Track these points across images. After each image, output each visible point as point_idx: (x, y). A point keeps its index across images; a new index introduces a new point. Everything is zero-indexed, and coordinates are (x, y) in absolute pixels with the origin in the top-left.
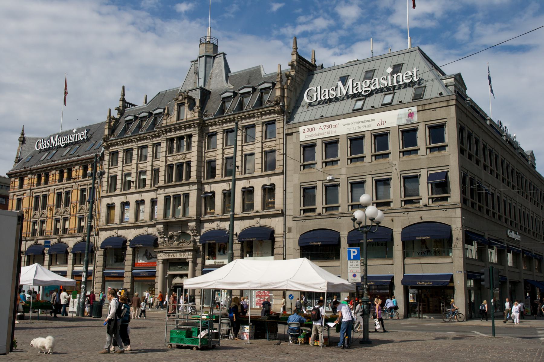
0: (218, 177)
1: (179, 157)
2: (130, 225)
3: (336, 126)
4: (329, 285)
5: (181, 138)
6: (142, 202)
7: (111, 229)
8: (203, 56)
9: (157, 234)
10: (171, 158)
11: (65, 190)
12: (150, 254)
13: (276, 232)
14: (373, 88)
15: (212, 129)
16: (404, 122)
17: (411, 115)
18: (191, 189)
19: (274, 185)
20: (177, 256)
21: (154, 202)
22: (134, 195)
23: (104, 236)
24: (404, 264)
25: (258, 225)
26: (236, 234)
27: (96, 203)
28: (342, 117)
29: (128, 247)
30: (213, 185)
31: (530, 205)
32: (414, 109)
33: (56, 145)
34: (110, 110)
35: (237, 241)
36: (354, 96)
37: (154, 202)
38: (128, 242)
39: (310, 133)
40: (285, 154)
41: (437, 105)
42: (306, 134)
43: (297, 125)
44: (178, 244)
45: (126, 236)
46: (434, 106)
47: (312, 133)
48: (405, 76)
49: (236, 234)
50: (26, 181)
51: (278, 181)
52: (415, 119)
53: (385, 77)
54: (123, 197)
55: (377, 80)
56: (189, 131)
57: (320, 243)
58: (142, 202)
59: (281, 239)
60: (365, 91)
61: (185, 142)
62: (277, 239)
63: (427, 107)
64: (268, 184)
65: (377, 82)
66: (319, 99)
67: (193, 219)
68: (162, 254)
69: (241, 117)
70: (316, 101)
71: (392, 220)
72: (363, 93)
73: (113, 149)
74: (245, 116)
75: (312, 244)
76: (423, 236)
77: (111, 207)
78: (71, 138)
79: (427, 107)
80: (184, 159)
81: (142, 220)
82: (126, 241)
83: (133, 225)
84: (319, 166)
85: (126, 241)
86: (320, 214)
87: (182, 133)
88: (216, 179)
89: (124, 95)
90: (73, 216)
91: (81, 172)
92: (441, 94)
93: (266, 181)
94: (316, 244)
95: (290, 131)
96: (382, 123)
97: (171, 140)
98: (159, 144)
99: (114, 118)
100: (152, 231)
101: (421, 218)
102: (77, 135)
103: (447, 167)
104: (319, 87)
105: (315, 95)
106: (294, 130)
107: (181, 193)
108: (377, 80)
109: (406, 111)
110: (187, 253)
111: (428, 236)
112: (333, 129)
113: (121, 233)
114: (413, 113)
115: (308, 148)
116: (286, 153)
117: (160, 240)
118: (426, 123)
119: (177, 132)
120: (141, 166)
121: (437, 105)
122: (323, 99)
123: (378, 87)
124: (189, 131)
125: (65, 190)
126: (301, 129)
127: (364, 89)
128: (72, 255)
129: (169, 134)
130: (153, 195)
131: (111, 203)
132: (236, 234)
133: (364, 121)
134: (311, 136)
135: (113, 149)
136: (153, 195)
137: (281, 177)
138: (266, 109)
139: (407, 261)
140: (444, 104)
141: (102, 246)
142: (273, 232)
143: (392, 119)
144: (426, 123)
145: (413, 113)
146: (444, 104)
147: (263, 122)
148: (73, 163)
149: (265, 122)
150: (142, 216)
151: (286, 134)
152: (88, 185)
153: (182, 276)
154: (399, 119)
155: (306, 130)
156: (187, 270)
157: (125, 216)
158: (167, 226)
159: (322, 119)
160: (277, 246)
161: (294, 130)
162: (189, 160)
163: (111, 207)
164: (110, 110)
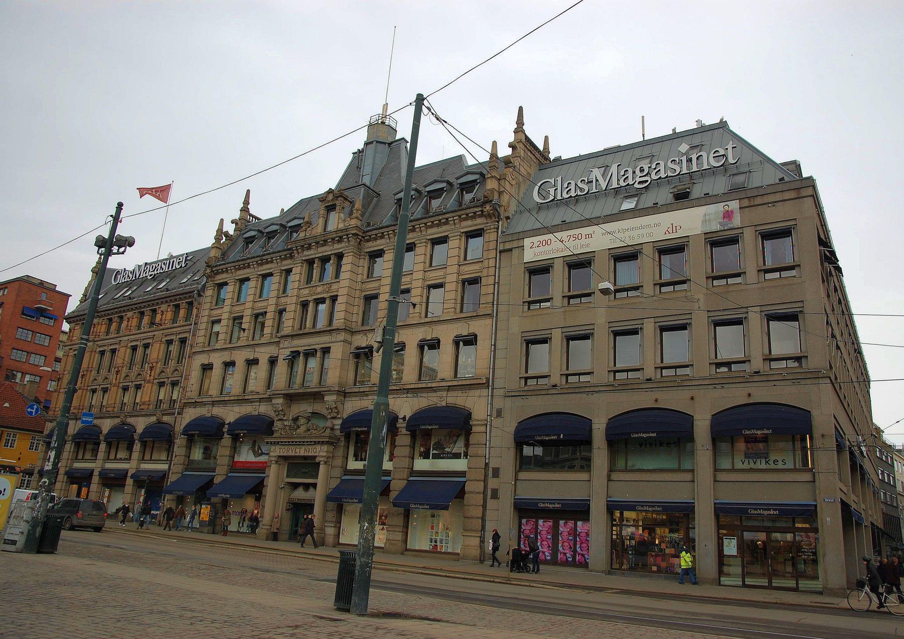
1: (319, 289)
2: (232, 398)
3: (589, 236)
5: (325, 260)
6: (232, 364)
7: (203, 404)
8: (372, 142)
9: (273, 414)
10: (306, 292)
12: (259, 448)
13: (474, 416)
14: (654, 177)
15: (410, 238)
16: (715, 227)
17: (728, 215)
18: (334, 340)
19: (476, 336)
20: (301, 451)
21: (273, 362)
23: (190, 414)
24: (516, 480)
25: (209, 415)
26: (405, 417)
27: (186, 361)
28: (594, 221)
29: (226, 435)
32: (734, 205)
35: (404, 431)
36: (617, 191)
37: (273, 362)
38: (227, 426)
39: (542, 249)
40: (497, 283)
41: (778, 197)
42: (535, 250)
43: (521, 236)
44: (305, 431)
45: (224, 417)
46: (772, 198)
47: (547, 248)
48: (712, 155)
49: (404, 419)
51: (482, 328)
52: (737, 221)
53: (586, 179)
54: (227, 353)
55: (662, 163)
56: (338, 248)
57: (654, 435)
58: (232, 364)
59: (483, 429)
60: (640, 183)
61: (330, 267)
62: (474, 429)
63: (758, 201)
65: (662, 167)
66: (559, 197)
67: (332, 389)
68: (278, 447)
69: (426, 224)
70: (553, 200)
71: (692, 398)
72: (636, 185)
73: (220, 278)
74: (433, 222)
76: (644, 433)
77: (207, 368)
79: (758, 201)
80: (328, 292)
81: (252, 392)
82: (223, 424)
84: (558, 301)
85: (223, 424)
86: (555, 386)
87: (327, 250)
90: (149, 382)
92: (782, 179)
94: (645, 436)
95: (508, 246)
96: (674, 228)
97: (311, 262)
98: (289, 271)
99: (227, 234)
100: (263, 409)
101: (656, 400)
103: (591, 327)
104: (559, 179)
105: (552, 191)
106: (515, 244)
107: (316, 347)
108: (662, 163)
109: (720, 207)
110: (318, 447)
111: (653, 432)
112: (584, 241)
113: (217, 411)
114: (732, 212)
115: (540, 270)
116: (498, 283)
117: (278, 425)
118: (759, 228)
119: (320, 249)
120: (214, 312)
121: (778, 197)
122: (565, 196)
123: (663, 175)
124: (338, 248)
126: (527, 242)
127: (638, 180)
128: (139, 445)
129: (306, 253)
130: (272, 350)
131: (207, 363)
132: (405, 417)
133: (642, 227)
134: (545, 253)
135: (220, 278)
136: (272, 350)
137: (488, 321)
138: (468, 211)
139: (523, 475)
140: (793, 195)
141: (185, 432)
142: (469, 415)
143: (691, 222)
144: (759, 228)
145: (732, 212)
146: (793, 195)
148: (125, 308)
149: (465, 232)
150: (252, 386)
151: (500, 252)
153: (307, 487)
154: (704, 221)
155: (536, 244)
156: (316, 476)
157: (227, 385)
158: (291, 398)
159: (565, 226)
160: (476, 442)
161: (515, 244)
162: (335, 294)
163: (207, 368)
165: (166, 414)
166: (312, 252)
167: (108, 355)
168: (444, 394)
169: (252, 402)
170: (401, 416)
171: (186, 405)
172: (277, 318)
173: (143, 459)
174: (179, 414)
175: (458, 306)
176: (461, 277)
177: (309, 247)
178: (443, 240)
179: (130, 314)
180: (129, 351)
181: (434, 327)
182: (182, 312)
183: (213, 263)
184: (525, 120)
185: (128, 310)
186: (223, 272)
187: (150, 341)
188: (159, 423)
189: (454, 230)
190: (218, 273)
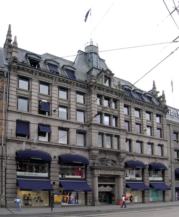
80: (112, 113)
89: (9, 31)
174: (4, 145)
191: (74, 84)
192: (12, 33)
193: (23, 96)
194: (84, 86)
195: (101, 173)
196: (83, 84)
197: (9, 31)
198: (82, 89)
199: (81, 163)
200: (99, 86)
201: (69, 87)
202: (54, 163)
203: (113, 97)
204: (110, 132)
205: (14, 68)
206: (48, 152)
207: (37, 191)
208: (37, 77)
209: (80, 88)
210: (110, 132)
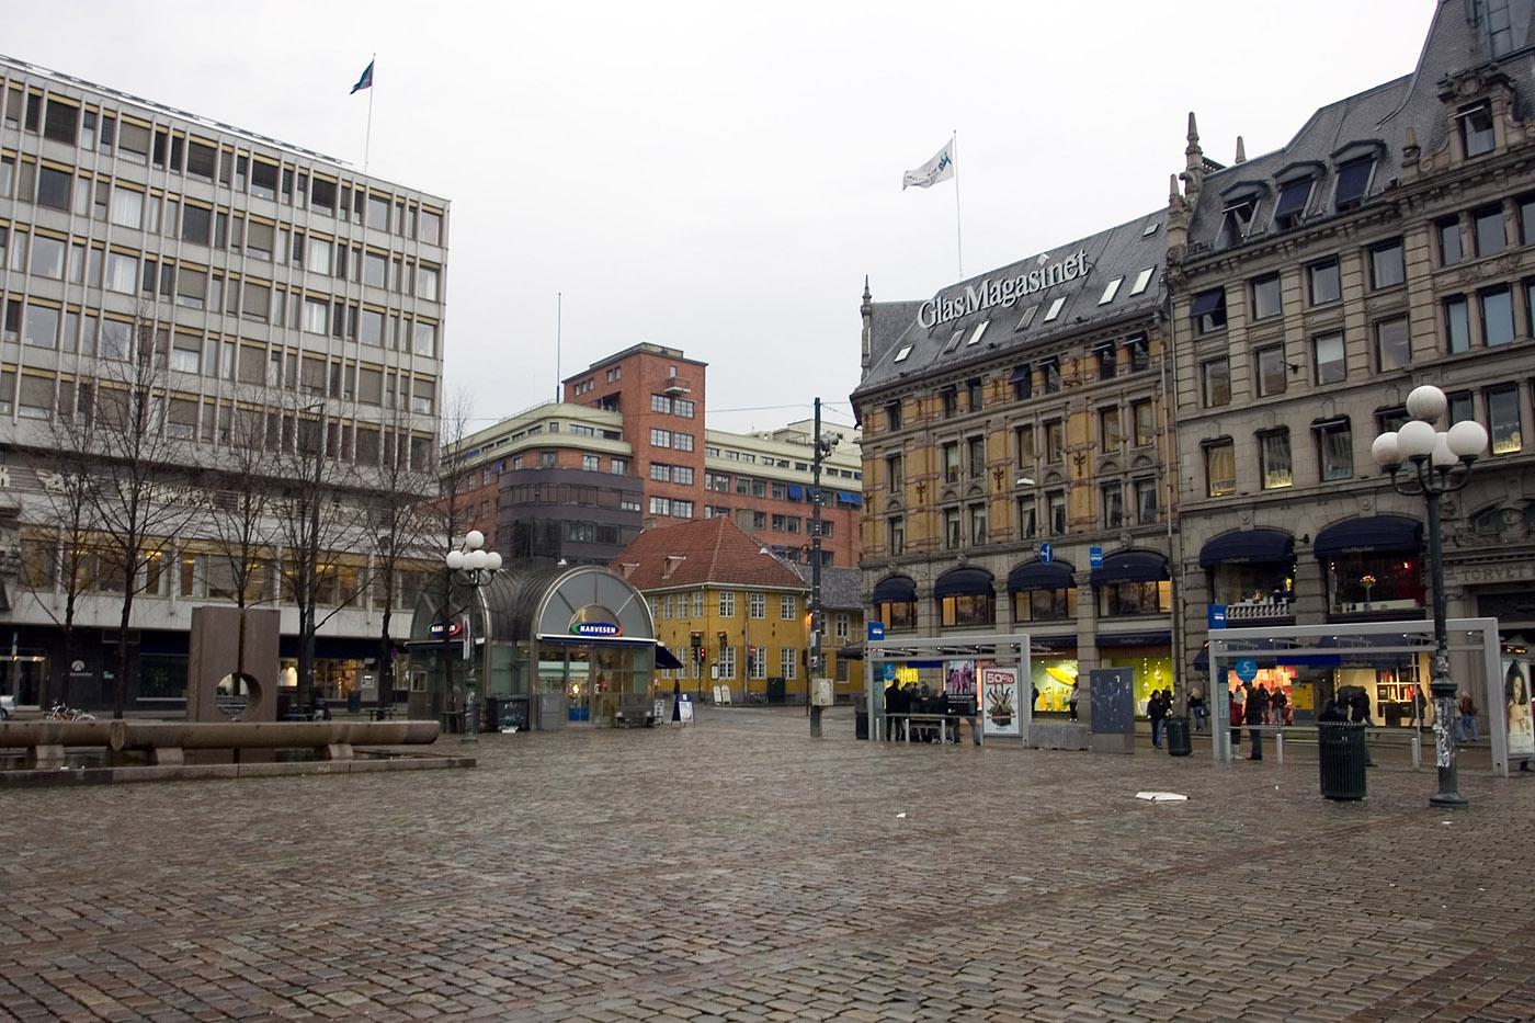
0: (1237, 402)
4: (62, 592)
11: (1041, 419)
19: (1347, 418)
22: (1304, 407)
26: (1306, 536)
30: (1224, 422)
31: (211, 604)
33: (985, 305)
34: (1240, 139)
49: (1306, 539)
50: (909, 413)
64: (1329, 416)
68: (1456, 569)
73: (1202, 283)
75: (1347, 551)
78: (1031, 280)
80: (1513, 272)
83: (1315, 492)
88: (1291, 394)
89: (1193, 137)
90: (1080, 484)
91: (1091, 364)
93: (1264, 422)
102: (1051, 269)
125: (1041, 419)
147: (1363, 247)
149: (1369, 246)
152: (1122, 395)
164: (1240, 139)
165: (1140, 536)
166: (1449, 200)
167: (1039, 435)
168: (1250, 512)
169: (1236, 511)
170: (1299, 535)
171: (1185, 515)
172: (1371, 336)
173: (1100, 616)
174: (1174, 531)
175: (1201, 401)
176: (1309, 333)
177: (1444, 191)
178: (1332, 261)
179: (995, 374)
180: (1012, 437)
181: (1277, 411)
182: (962, 399)
183: (1180, 258)
184: (1200, 132)
185: (992, 367)
186: (1208, 269)
187: (982, 432)
188: (964, 569)
189: (1287, 262)
190: (1197, 273)
191: (1346, 229)
192: (1199, 144)
193: (1269, 342)
194: (1382, 214)
195: (1471, 581)
196: (1375, 211)
197: (1193, 137)
198: (1386, 225)
199: (1371, 549)
200: (1422, 189)
201: (1496, 193)
202: (1306, 563)
203: (1507, 194)
204: (1496, 377)
205: (1179, 283)
206: (1287, 527)
207: (253, 411)
208: (1352, 237)
209: (1377, 228)
210: (1496, 377)
